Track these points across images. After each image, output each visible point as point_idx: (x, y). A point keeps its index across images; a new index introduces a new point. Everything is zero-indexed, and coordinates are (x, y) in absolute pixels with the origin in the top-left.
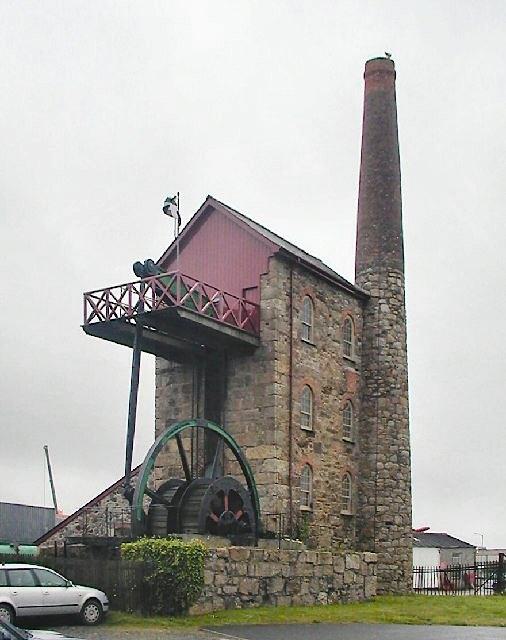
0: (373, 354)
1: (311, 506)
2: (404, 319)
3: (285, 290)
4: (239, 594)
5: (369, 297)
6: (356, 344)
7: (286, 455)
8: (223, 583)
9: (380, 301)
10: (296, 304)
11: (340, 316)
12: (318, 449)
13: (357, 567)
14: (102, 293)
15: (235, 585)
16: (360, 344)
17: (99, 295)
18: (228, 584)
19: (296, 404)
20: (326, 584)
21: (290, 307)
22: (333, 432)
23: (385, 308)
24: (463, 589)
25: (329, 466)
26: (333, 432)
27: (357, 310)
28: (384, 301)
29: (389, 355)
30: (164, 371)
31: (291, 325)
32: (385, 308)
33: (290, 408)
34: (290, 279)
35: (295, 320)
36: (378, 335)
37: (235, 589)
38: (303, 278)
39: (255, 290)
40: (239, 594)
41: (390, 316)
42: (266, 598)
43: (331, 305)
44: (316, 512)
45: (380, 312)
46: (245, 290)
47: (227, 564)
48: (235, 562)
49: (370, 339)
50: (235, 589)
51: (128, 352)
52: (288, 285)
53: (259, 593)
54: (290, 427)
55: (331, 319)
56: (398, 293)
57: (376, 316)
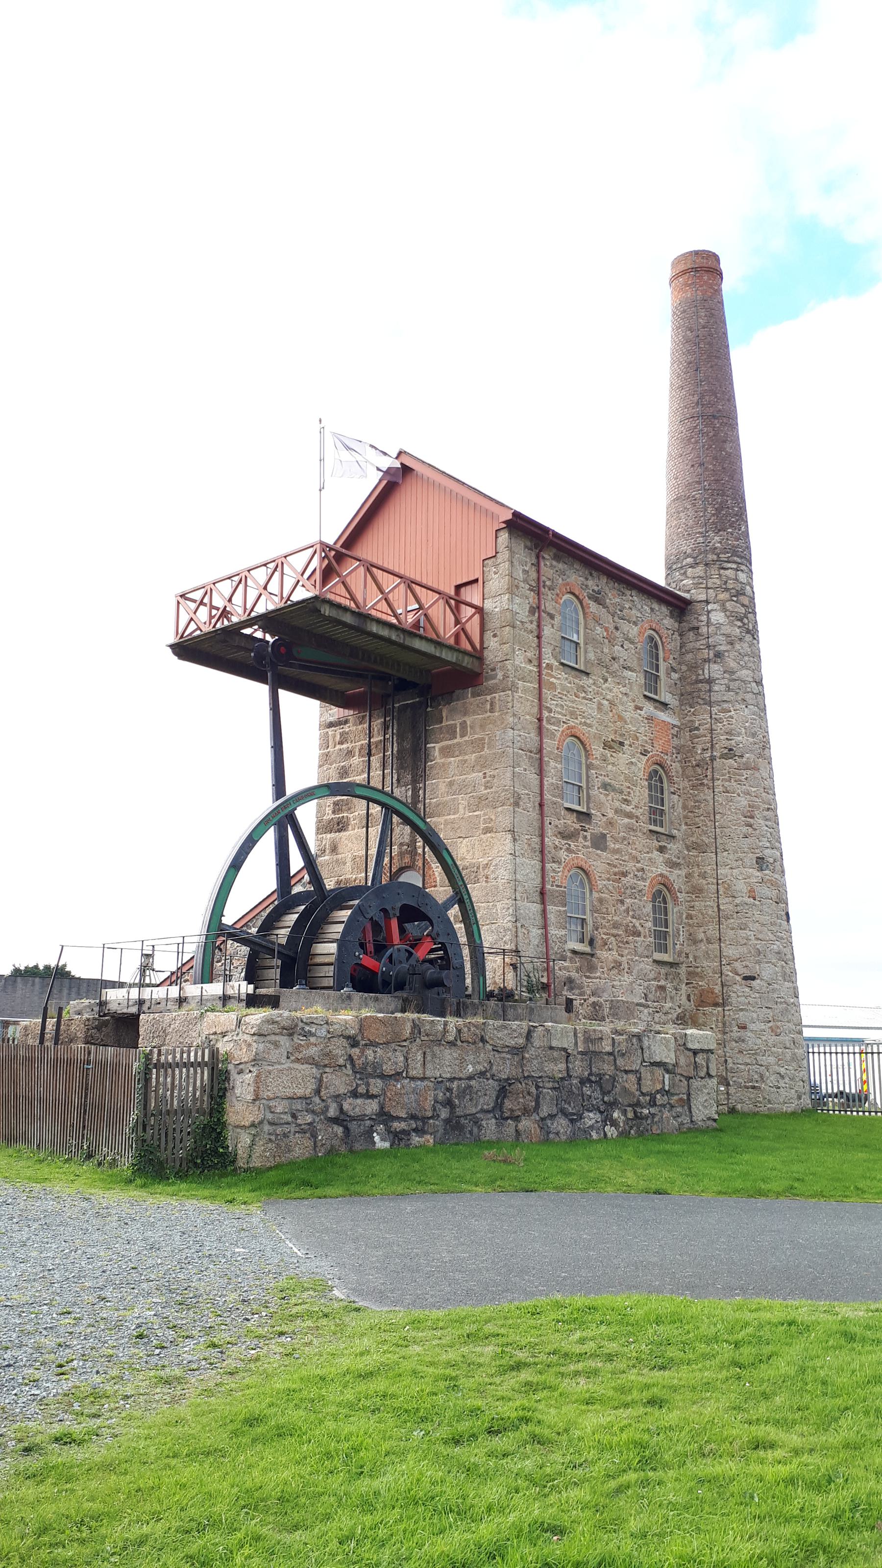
0: (700, 690)
1: (591, 942)
2: (753, 632)
3: (525, 581)
4: (384, 1116)
5: (687, 603)
6: (668, 674)
7: (533, 850)
8: (343, 1090)
9: (710, 607)
10: (549, 605)
11: (636, 629)
12: (599, 842)
13: (670, 1059)
14: (202, 591)
15: (373, 1097)
16: (675, 676)
17: (197, 595)
18: (355, 1094)
19: (552, 766)
20: (597, 1094)
21: (536, 609)
22: (629, 815)
23: (718, 617)
24: (640, 1073)
25: (625, 874)
26: (629, 815)
27: (668, 622)
28: (715, 606)
29: (729, 689)
30: (331, 725)
31: (539, 637)
32: (718, 617)
33: (541, 773)
34: (537, 566)
35: (547, 631)
36: (708, 660)
37: (372, 1107)
38: (560, 566)
39: (475, 585)
40: (384, 1116)
41: (727, 629)
42: (454, 1125)
43: (617, 613)
44: (602, 954)
45: (708, 623)
46: (458, 588)
47: (356, 1051)
48: (373, 1044)
49: (693, 667)
50: (372, 1107)
51: (262, 690)
52: (533, 575)
53: (436, 1116)
54: (541, 805)
55: (618, 634)
56: (740, 593)
57: (704, 630)
